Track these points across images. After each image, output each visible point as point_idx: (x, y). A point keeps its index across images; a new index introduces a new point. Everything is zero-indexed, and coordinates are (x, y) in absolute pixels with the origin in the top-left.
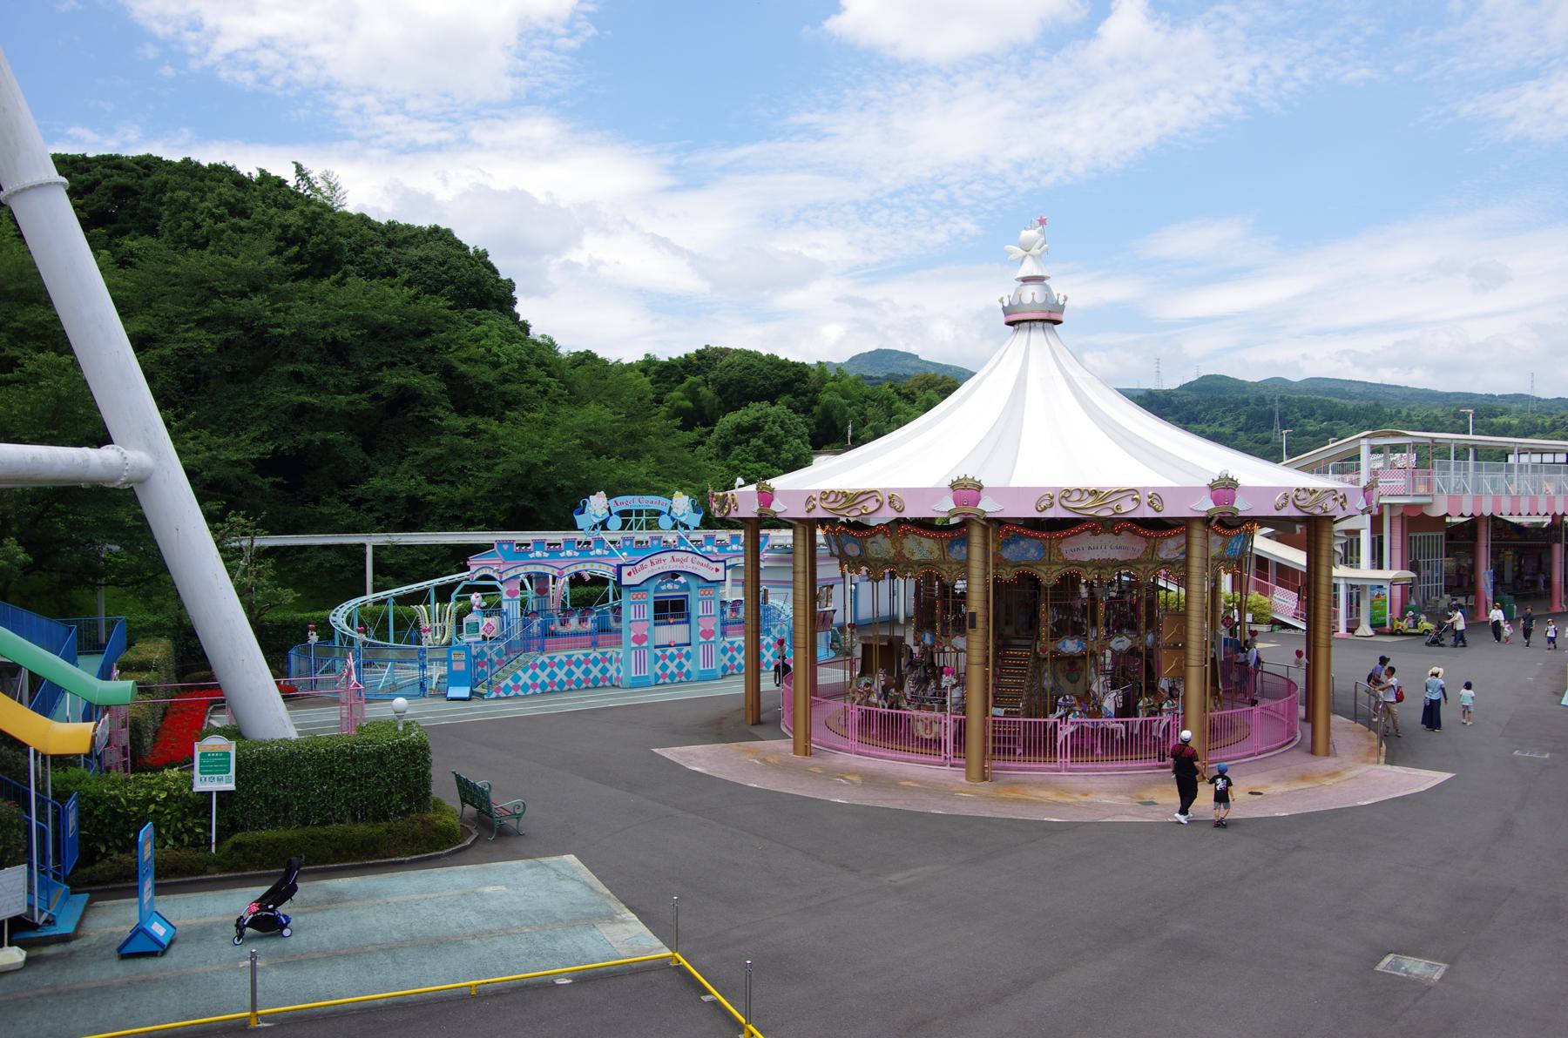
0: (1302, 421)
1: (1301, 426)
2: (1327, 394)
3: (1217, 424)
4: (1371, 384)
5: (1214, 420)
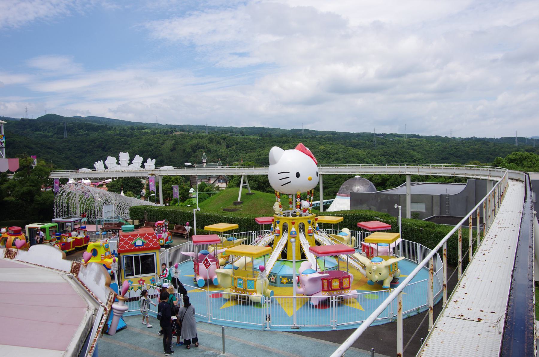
0: (78, 130)
1: (78, 132)
2: (93, 122)
3: (47, 132)
4: (110, 119)
5: (46, 130)
